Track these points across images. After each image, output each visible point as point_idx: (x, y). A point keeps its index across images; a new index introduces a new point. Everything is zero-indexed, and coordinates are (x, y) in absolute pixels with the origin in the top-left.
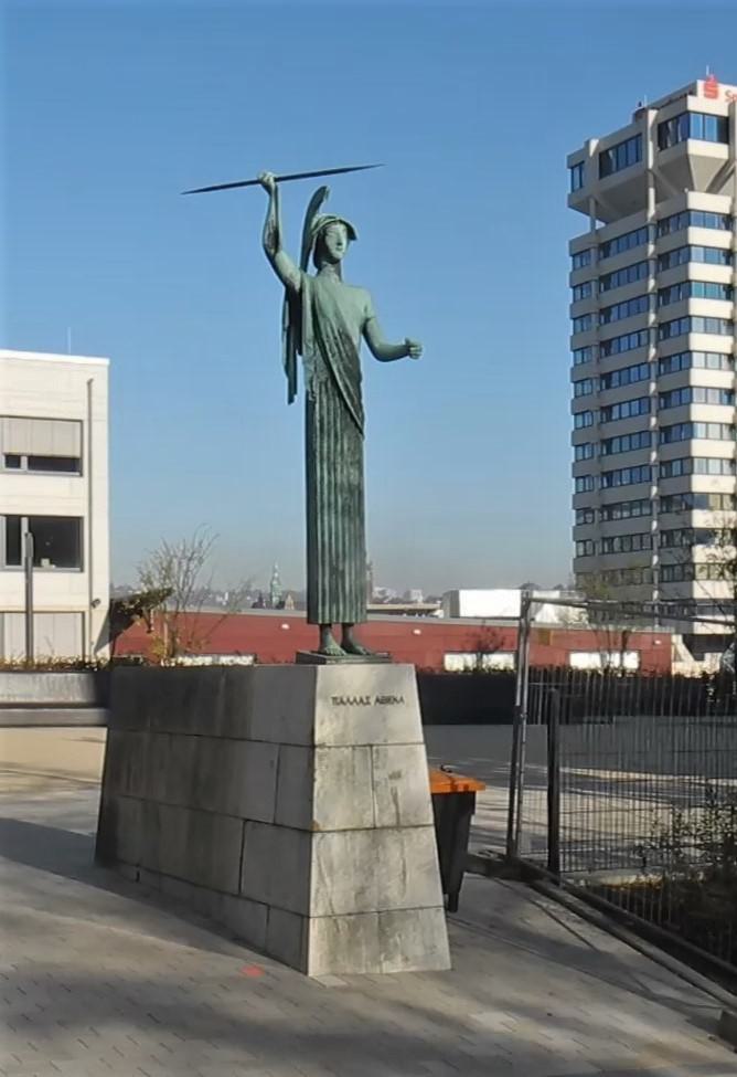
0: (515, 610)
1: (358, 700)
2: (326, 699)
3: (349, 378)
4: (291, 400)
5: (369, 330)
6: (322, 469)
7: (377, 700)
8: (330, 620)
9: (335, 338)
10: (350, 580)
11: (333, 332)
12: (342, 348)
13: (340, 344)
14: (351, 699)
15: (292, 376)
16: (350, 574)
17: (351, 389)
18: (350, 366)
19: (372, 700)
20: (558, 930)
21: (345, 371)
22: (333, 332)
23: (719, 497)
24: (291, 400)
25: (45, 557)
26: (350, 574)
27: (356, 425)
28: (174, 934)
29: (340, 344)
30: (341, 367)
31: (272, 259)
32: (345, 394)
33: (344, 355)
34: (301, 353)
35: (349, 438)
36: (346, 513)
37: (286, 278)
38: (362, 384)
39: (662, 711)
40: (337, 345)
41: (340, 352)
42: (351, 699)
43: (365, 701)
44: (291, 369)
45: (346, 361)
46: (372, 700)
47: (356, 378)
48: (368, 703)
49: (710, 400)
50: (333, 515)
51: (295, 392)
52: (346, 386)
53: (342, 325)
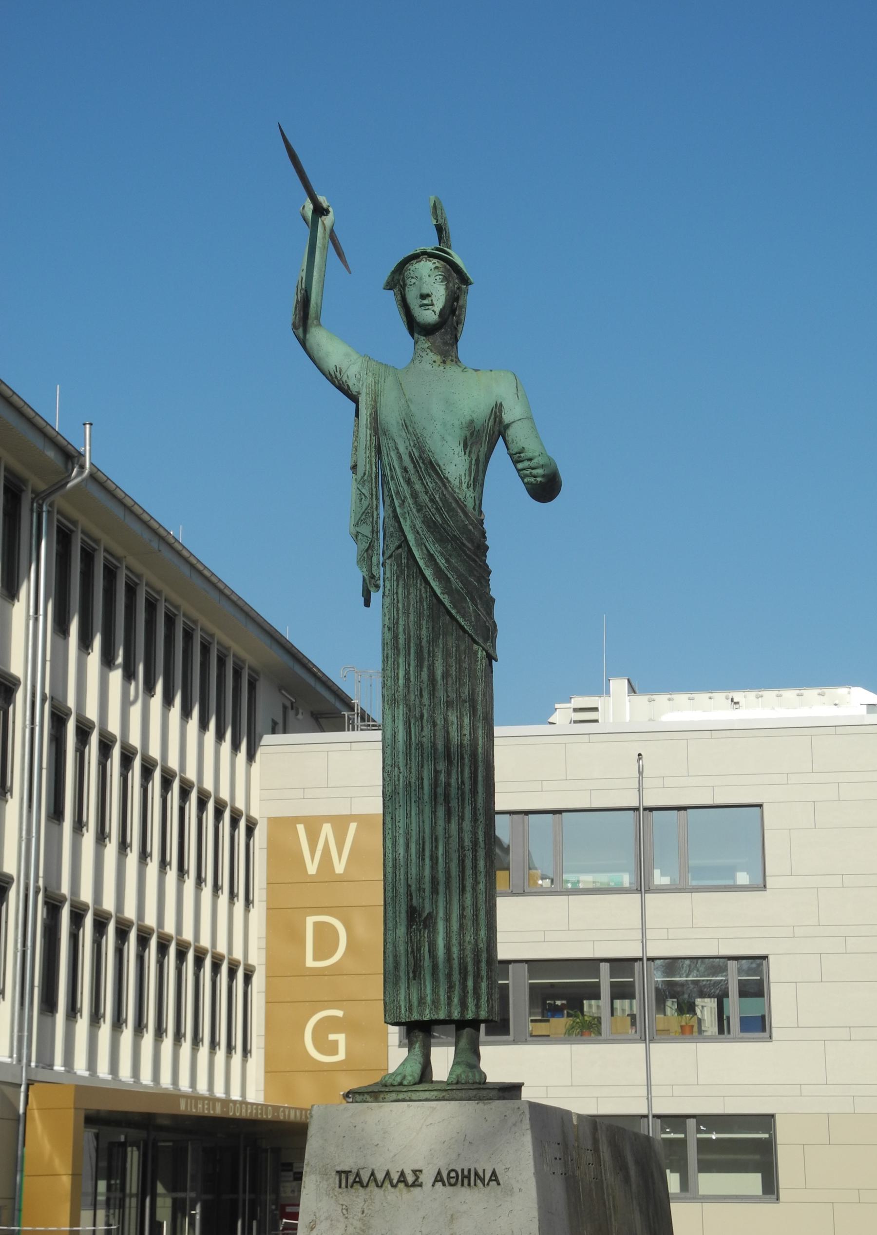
0: (396, 1029)
1: (395, 1177)
2: (324, 1174)
7: (439, 1178)
9: (405, 470)
10: (448, 934)
11: (400, 458)
12: (418, 487)
13: (414, 478)
14: (380, 1176)
16: (448, 919)
17: (441, 562)
19: (427, 1178)
22: (400, 458)
25: (618, 675)
26: (448, 919)
29: (414, 478)
30: (419, 524)
31: (303, 343)
32: (428, 573)
33: (424, 498)
35: (447, 655)
36: (441, 799)
37: (332, 369)
39: (343, 1185)
40: (409, 482)
41: (415, 495)
42: (380, 1176)
43: (410, 1179)
46: (427, 1178)
48: (417, 1184)
52: (431, 557)
53: (419, 444)
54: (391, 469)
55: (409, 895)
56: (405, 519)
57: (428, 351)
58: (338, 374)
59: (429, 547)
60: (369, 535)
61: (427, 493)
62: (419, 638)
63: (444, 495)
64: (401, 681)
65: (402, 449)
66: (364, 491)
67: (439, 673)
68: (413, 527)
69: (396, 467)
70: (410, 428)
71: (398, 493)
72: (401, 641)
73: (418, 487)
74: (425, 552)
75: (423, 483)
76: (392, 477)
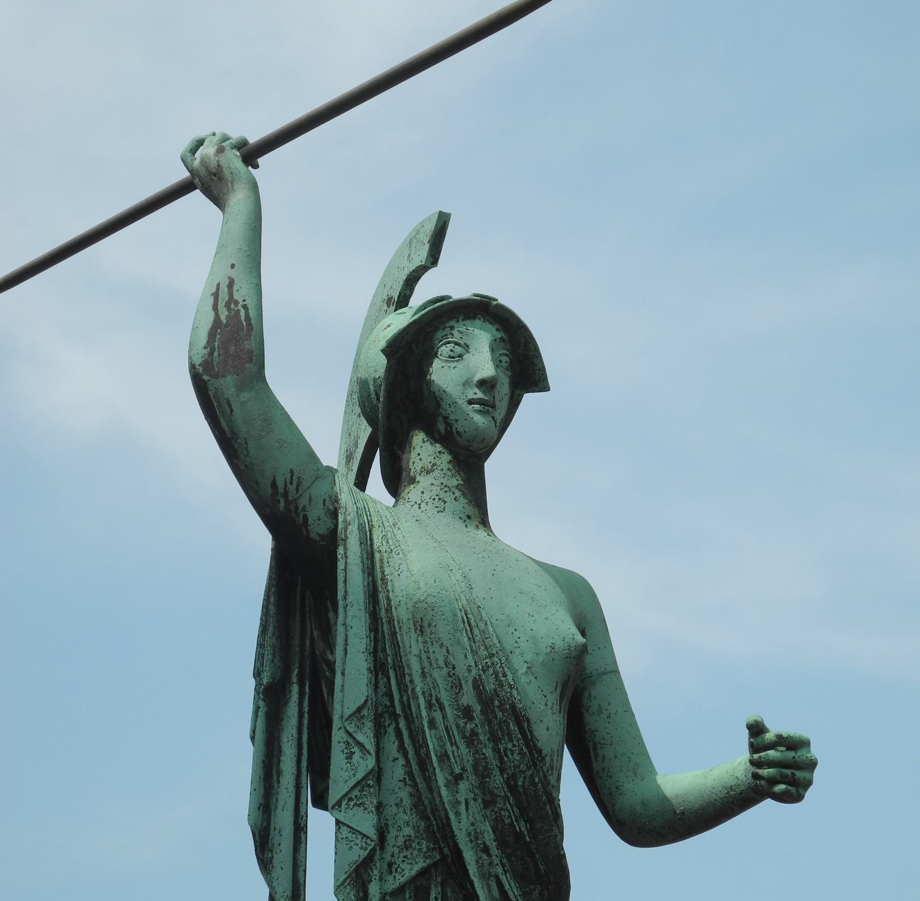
11: (457, 686)
33: (497, 780)
38: (767, 809)
41: (482, 772)
45: (508, 810)
54: (430, 706)
56: (458, 814)
57: (458, 493)
58: (292, 489)
59: (507, 887)
60: (372, 833)
61: (502, 770)
63: (534, 784)
65: (461, 670)
66: (360, 737)
68: (475, 837)
70: (476, 632)
71: (444, 757)
73: (489, 752)
75: (496, 750)
76: (432, 724)
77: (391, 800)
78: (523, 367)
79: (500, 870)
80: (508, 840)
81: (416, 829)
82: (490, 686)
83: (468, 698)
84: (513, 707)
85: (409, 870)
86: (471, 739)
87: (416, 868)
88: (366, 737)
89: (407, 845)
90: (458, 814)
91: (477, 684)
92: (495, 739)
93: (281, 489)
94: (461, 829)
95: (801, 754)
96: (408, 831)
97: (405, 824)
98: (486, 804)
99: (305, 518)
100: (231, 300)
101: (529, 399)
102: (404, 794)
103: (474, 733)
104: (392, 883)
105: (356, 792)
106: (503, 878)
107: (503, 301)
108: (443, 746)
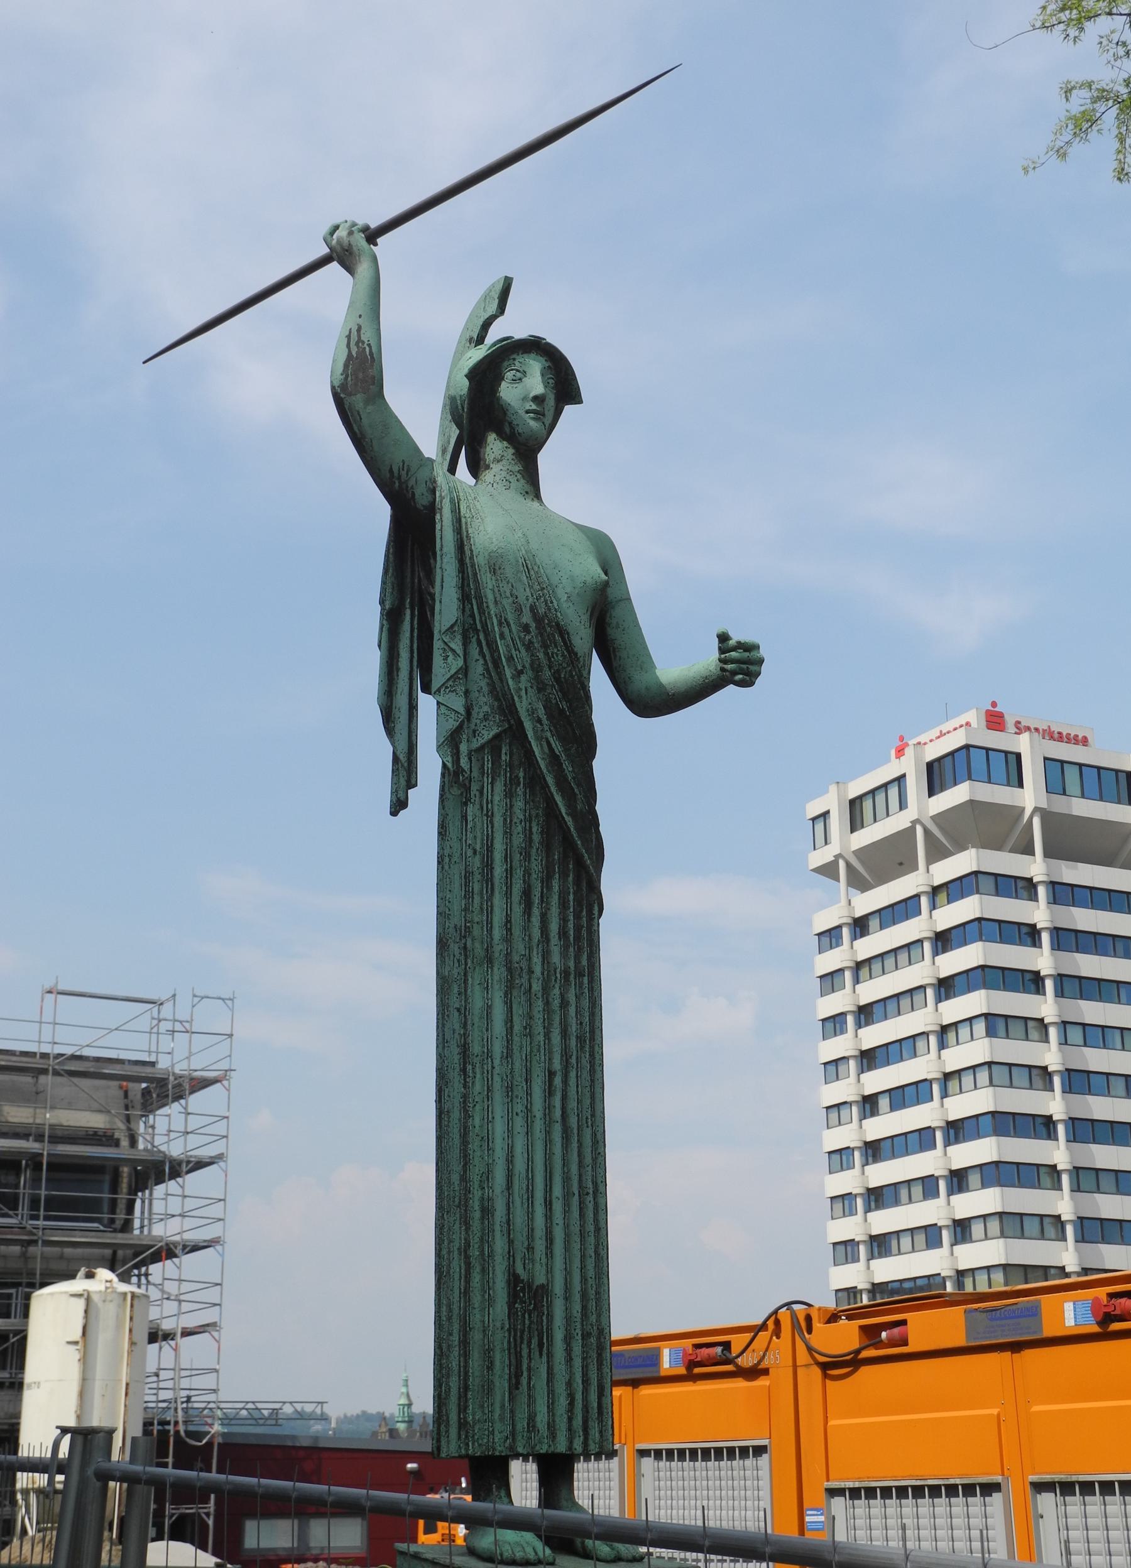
3: (562, 739)
4: (399, 805)
5: (612, 632)
6: (530, 1160)
8: (570, 1448)
11: (519, 610)
15: (403, 746)
17: (567, 767)
18: (564, 705)
20: (672, 1559)
21: (550, 717)
23: (1086, 1238)
24: (399, 805)
27: (579, 863)
28: (72, 1123)
33: (547, 674)
34: (426, 689)
41: (536, 669)
44: (396, 716)
45: (555, 694)
47: (582, 742)
49: (1047, 1235)
50: (519, 1123)
51: (411, 783)
52: (554, 759)
55: (511, 1256)
56: (520, 697)
58: (404, 473)
61: (550, 668)
62: (527, 873)
64: (497, 933)
65: (522, 599)
66: (453, 645)
67: (554, 927)
68: (532, 712)
69: (511, 622)
70: (532, 572)
71: (510, 659)
72: (499, 871)
74: (546, 750)
75: (546, 654)
76: (502, 636)
77: (474, 688)
78: (564, 387)
79: (549, 734)
80: (554, 713)
81: (492, 707)
82: (542, 610)
83: (527, 618)
84: (558, 624)
85: (487, 735)
86: (529, 646)
87: (492, 734)
88: (457, 645)
89: (486, 718)
90: (520, 697)
91: (533, 609)
92: (545, 646)
93: (396, 474)
94: (522, 707)
95: (754, 654)
96: (486, 708)
97: (484, 704)
98: (540, 690)
99: (413, 494)
100: (359, 341)
101: (568, 409)
102: (483, 683)
103: (531, 642)
104: (475, 744)
105: (450, 683)
106: (551, 739)
107: (550, 340)
108: (509, 651)
